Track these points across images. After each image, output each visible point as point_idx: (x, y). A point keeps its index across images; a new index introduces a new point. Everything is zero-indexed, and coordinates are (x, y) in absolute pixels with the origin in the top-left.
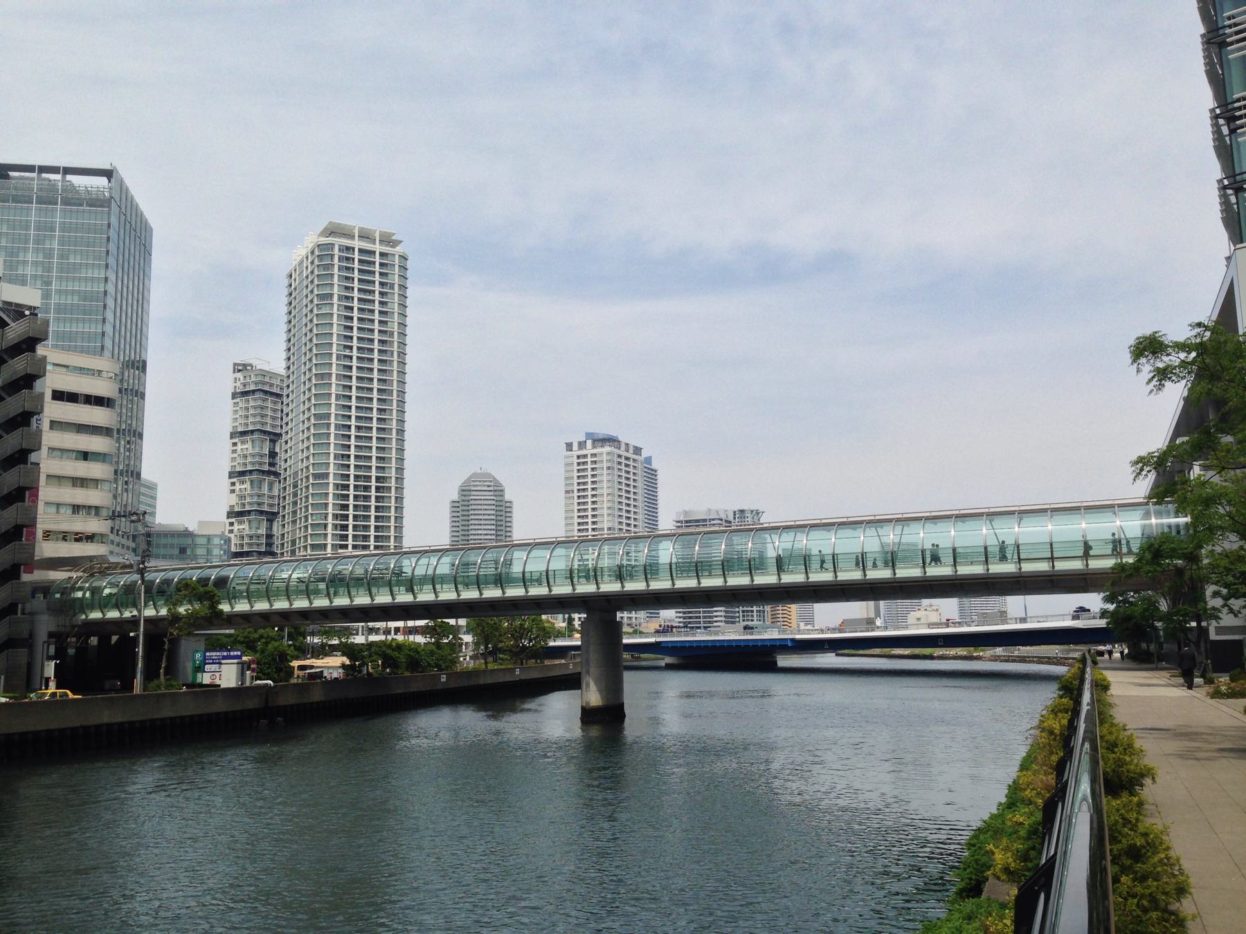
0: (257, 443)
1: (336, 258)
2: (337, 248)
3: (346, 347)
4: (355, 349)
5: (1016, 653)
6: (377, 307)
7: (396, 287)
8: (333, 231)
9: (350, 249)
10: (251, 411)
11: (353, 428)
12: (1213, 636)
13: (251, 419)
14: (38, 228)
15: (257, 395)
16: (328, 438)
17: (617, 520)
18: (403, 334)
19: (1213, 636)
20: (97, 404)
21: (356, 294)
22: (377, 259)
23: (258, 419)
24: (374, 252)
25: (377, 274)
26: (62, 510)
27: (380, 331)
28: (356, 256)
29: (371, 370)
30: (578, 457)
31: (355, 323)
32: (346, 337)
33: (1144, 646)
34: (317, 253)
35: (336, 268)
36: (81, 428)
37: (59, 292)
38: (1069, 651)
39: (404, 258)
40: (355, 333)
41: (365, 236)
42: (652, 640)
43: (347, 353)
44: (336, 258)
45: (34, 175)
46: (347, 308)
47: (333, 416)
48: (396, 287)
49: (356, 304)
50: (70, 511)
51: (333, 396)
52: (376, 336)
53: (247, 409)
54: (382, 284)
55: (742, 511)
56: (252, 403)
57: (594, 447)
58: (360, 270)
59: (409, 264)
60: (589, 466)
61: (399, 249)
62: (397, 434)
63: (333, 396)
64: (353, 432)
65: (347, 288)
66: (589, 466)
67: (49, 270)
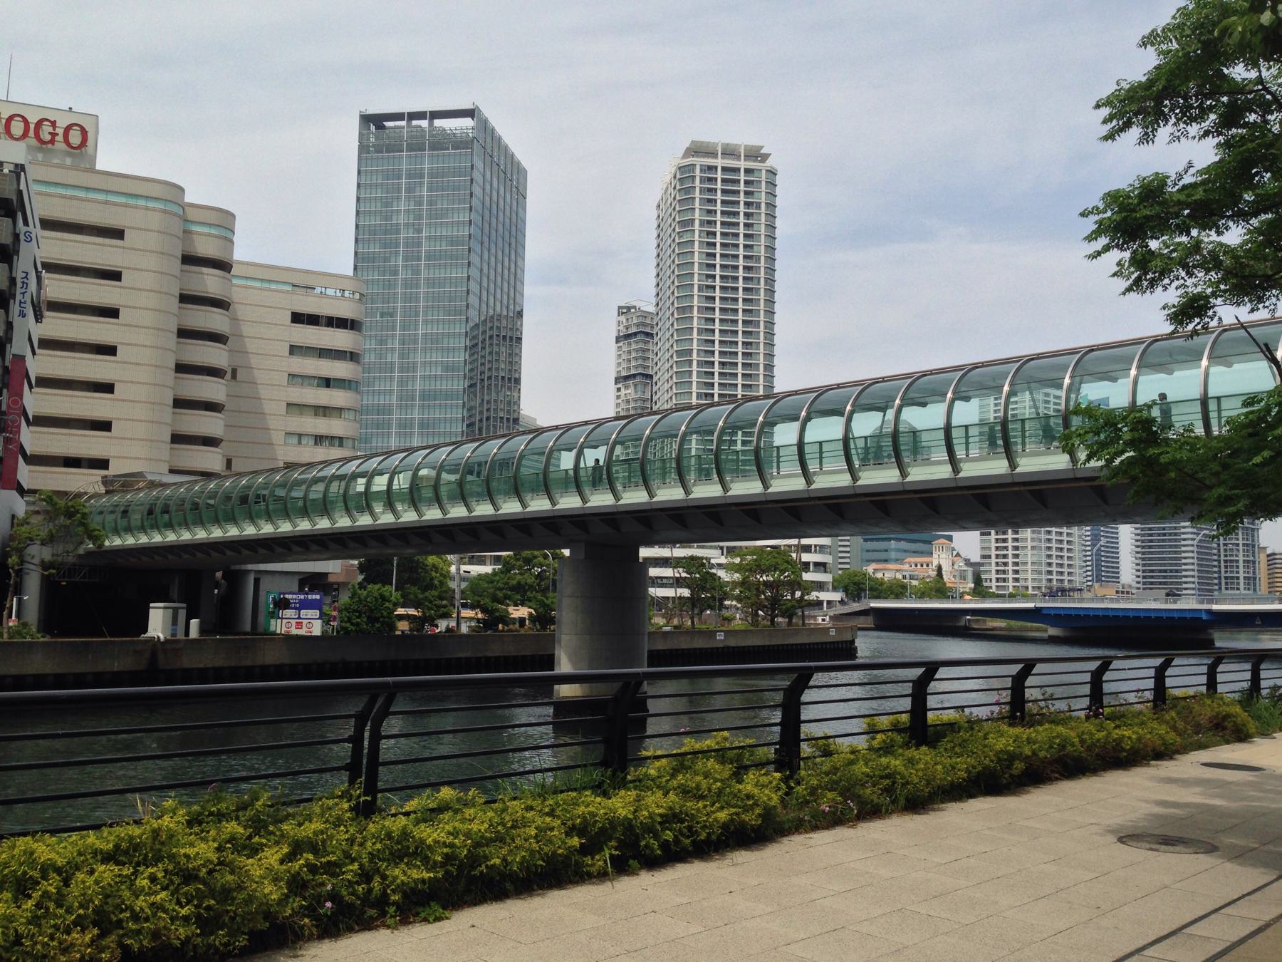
0: (639, 388)
1: (698, 180)
3: (708, 276)
6: (742, 230)
7: (763, 206)
8: (696, 150)
9: (712, 168)
10: (634, 355)
11: (716, 364)
13: (633, 363)
14: (409, 176)
15: (639, 338)
16: (690, 376)
18: (771, 259)
20: (338, 327)
21: (719, 218)
22: (742, 177)
23: (640, 362)
24: (739, 170)
26: (304, 441)
27: (745, 257)
28: (719, 176)
29: (736, 300)
31: (718, 250)
32: (708, 265)
34: (678, 176)
35: (698, 190)
36: (324, 353)
37: (429, 238)
39: (772, 173)
41: (729, 152)
42: (1031, 605)
43: (710, 282)
44: (698, 180)
45: (403, 123)
46: (709, 233)
47: (695, 353)
48: (763, 206)
49: (718, 229)
50: (312, 442)
51: (695, 331)
53: (629, 352)
54: (747, 204)
56: (634, 346)
59: (778, 180)
62: (765, 369)
63: (695, 331)
64: (717, 369)
67: (420, 217)
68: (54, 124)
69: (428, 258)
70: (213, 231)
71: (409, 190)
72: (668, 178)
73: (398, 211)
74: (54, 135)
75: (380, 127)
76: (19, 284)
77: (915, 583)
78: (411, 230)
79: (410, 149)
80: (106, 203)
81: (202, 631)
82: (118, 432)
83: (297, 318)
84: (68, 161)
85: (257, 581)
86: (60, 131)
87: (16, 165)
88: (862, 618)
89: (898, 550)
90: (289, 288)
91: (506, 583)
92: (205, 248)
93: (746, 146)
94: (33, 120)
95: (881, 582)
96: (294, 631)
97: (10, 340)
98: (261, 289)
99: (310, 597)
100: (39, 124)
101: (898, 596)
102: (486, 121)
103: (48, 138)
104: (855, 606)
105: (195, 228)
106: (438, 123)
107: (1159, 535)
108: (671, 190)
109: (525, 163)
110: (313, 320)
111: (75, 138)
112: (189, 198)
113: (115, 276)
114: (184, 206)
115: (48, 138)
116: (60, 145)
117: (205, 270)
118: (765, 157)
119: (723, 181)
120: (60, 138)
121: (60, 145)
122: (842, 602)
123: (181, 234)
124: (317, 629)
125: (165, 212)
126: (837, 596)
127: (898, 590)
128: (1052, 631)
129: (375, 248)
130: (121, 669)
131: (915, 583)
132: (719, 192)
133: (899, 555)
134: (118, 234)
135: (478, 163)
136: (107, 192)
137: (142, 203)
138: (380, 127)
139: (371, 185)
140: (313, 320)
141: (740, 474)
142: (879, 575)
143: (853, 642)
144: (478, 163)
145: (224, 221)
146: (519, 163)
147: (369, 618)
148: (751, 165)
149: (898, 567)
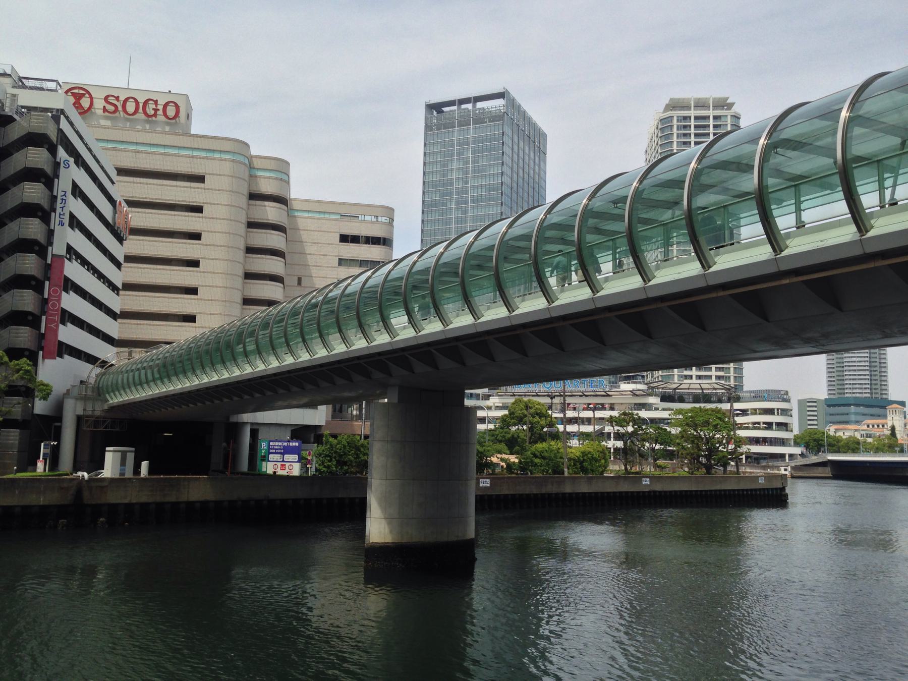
1: (675, 127)
8: (674, 105)
9: (686, 118)
20: (374, 243)
22: (711, 122)
24: (708, 117)
35: (675, 135)
44: (675, 127)
45: (455, 108)
67: (467, 173)
68: (156, 102)
69: (473, 201)
70: (272, 175)
71: (459, 154)
72: (653, 129)
73: (452, 170)
74: (156, 110)
75: (440, 112)
76: (59, 201)
77: (870, 440)
78: (461, 183)
79: (460, 125)
80: (192, 157)
81: (151, 471)
82: (141, 314)
83: (344, 239)
84: (167, 129)
85: (254, 434)
86: (160, 107)
87: (58, 110)
88: (820, 469)
89: (856, 414)
90: (338, 217)
91: (504, 437)
92: (267, 187)
93: (714, 99)
94: (141, 100)
95: (839, 440)
96: (280, 472)
97: (50, 243)
98: (319, 219)
99: (291, 444)
100: (146, 103)
101: (855, 450)
102: (514, 100)
103: (152, 112)
104: (814, 459)
105: (259, 173)
106: (480, 105)
108: (655, 138)
109: (545, 128)
110: (355, 239)
111: (171, 111)
112: (254, 151)
113: (198, 209)
114: (251, 158)
115: (152, 112)
116: (161, 118)
117: (266, 203)
118: (730, 106)
119: (696, 127)
120: (160, 112)
121: (161, 118)
122: (802, 455)
123: (247, 178)
124: (296, 470)
125: (233, 161)
126: (797, 450)
127: (853, 446)
129: (436, 197)
130: (47, 503)
131: (870, 440)
132: (693, 136)
133: (859, 418)
134: (200, 179)
135: (508, 130)
136: (193, 149)
137: (217, 155)
138: (440, 112)
139: (433, 153)
140: (355, 239)
142: (840, 434)
143: (783, 489)
144: (508, 130)
145: (282, 168)
146: (540, 129)
147: (338, 462)
148: (718, 112)
149: (856, 427)
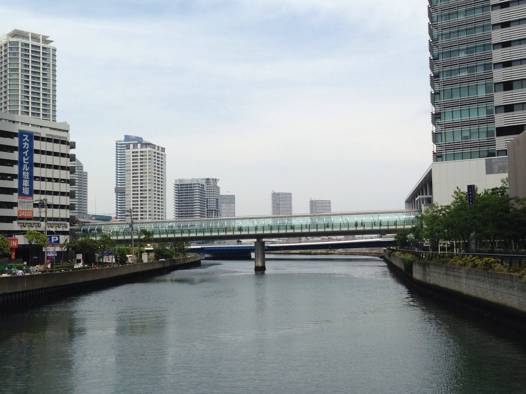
2: (20, 44)
4: (30, 98)
5: (349, 251)
6: (41, 76)
8: (16, 34)
12: (424, 245)
17: (153, 185)
19: (424, 245)
21: (30, 69)
22: (41, 51)
24: (39, 47)
25: (41, 59)
28: (30, 48)
30: (133, 152)
33: (80, 256)
38: (372, 250)
39: (55, 50)
40: (30, 90)
41: (35, 37)
42: (200, 247)
49: (30, 74)
52: (41, 91)
54: (43, 64)
55: (208, 179)
57: (142, 147)
58: (32, 56)
59: (57, 53)
60: (139, 158)
61: (51, 45)
65: (25, 65)
66: (139, 158)
107: (185, 214)
128: (207, 256)
132: (30, 57)
141: (282, 229)
